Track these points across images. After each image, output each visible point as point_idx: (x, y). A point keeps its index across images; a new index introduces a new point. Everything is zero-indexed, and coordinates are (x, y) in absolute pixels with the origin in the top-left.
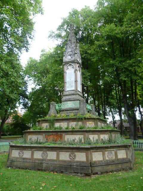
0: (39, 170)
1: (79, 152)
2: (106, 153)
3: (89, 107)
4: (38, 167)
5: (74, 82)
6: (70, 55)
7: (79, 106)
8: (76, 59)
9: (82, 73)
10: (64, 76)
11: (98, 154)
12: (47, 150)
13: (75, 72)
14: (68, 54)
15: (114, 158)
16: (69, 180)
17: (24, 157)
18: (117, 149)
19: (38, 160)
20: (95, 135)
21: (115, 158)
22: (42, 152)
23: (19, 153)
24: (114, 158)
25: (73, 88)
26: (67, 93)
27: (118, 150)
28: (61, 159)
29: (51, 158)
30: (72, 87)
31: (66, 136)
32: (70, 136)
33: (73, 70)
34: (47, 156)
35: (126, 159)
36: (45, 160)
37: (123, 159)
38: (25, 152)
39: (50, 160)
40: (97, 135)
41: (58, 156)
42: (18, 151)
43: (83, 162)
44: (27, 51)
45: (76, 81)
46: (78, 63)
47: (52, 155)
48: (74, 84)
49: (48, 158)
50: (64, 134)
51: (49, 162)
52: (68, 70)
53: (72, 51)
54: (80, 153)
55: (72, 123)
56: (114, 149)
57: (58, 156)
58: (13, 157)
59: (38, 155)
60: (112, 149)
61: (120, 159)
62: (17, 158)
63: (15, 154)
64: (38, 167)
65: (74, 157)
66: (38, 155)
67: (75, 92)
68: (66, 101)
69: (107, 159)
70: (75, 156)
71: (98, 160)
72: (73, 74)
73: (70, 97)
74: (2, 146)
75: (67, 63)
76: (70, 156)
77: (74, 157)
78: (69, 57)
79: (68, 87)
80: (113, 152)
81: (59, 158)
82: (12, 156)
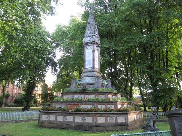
0: (61, 128)
1: (88, 116)
2: (108, 118)
3: (105, 82)
4: (60, 126)
5: (92, 60)
6: (89, 37)
7: (94, 81)
8: (94, 41)
9: (101, 51)
10: (84, 55)
11: (102, 118)
12: (66, 115)
13: (93, 52)
14: (87, 36)
15: (114, 121)
16: (47, 107)
17: (50, 120)
18: (118, 115)
19: (60, 121)
20: (103, 105)
21: (115, 122)
22: (63, 116)
23: (47, 117)
24: (114, 121)
25: (91, 66)
26: (86, 70)
27: (118, 116)
28: (76, 121)
29: (69, 121)
30: (90, 65)
31: (81, 105)
32: (84, 105)
33: (91, 50)
34: (66, 119)
35: (124, 123)
36: (65, 122)
37: (122, 123)
38: (51, 116)
39: (68, 122)
40: (104, 105)
41: (74, 119)
42: (46, 116)
43: (90, 123)
44: (52, 13)
45: (94, 60)
46: (96, 43)
47: (70, 119)
48: (92, 63)
49: (67, 121)
50: (79, 104)
51: (68, 124)
52: (87, 50)
53: (90, 33)
54: (89, 117)
55: (88, 95)
56: (115, 116)
57: (74, 119)
58: (43, 120)
59: (60, 118)
60: (113, 116)
61: (119, 122)
62: (45, 120)
63: (44, 117)
64: (60, 126)
65: (84, 120)
66: (60, 118)
67: (93, 70)
68: (35, 120)
69: (109, 122)
70: (85, 119)
71: (101, 122)
72: (92, 53)
73: (88, 74)
74: (22, 115)
75: (87, 44)
76: (82, 119)
77: (84, 120)
78: (89, 38)
79: (87, 65)
80: (114, 118)
81: (75, 121)
82: (42, 119)
